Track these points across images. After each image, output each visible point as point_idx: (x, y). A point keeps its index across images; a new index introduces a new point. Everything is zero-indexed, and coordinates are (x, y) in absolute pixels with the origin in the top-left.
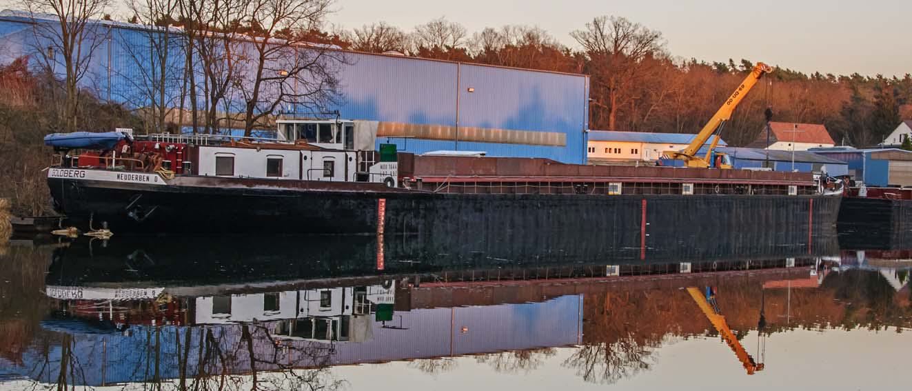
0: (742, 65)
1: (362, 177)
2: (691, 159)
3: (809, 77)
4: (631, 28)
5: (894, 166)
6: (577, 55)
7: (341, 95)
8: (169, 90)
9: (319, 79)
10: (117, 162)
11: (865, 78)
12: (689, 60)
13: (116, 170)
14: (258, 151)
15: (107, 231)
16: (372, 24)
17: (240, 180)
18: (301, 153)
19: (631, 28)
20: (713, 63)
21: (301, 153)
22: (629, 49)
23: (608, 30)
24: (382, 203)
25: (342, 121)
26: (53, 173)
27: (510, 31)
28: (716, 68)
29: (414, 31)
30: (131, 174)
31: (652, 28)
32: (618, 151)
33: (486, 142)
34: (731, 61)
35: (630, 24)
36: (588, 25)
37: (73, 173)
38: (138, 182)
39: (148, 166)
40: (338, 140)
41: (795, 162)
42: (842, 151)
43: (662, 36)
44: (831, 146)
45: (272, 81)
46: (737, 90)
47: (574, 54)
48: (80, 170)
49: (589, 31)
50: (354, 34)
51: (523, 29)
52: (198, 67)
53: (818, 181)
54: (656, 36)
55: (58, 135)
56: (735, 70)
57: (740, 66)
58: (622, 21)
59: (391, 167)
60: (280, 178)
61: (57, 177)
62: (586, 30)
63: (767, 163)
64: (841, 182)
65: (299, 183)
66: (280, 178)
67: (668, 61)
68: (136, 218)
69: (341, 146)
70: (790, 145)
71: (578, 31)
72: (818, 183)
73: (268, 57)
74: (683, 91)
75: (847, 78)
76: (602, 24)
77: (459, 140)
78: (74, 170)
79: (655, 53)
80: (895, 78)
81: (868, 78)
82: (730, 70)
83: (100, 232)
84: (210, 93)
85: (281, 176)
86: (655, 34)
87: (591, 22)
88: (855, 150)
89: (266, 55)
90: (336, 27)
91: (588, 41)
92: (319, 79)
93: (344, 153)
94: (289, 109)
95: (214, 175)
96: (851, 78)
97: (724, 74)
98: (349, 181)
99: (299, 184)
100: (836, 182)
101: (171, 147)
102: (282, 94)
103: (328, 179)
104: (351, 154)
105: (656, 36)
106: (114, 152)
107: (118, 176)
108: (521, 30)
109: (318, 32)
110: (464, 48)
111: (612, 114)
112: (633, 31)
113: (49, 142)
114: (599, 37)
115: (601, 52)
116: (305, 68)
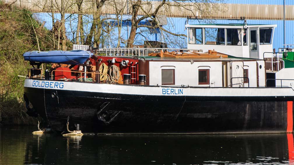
18: (257, 62)
21: (257, 62)
37: (53, 85)
48: (59, 82)
61: (38, 87)
77: (288, 19)
83: (74, 132)
113: (28, 58)
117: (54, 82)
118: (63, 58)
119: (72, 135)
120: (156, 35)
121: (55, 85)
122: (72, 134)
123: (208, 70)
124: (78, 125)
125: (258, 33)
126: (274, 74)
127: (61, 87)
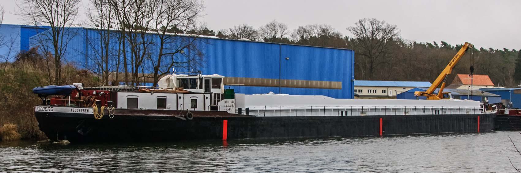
1: (215, 108)
2: (431, 96)
4: (380, 24)
6: (352, 40)
8: (110, 62)
10: (71, 102)
13: (71, 106)
14: (152, 94)
16: (239, 26)
17: (141, 111)
19: (380, 24)
23: (368, 26)
24: (225, 122)
25: (202, 76)
26: (39, 109)
28: (428, 46)
30: (79, 108)
31: (392, 24)
33: (297, 87)
34: (434, 42)
36: (356, 24)
37: (47, 109)
38: (82, 113)
39: (89, 104)
40: (201, 88)
45: (167, 55)
47: (350, 39)
48: (51, 107)
53: (483, 106)
54: (394, 28)
55: (40, 88)
59: (231, 102)
61: (39, 111)
62: (355, 26)
63: (472, 97)
64: (495, 107)
65: (177, 112)
68: (82, 133)
69: (202, 91)
71: (351, 27)
73: (165, 42)
76: (364, 22)
77: (282, 87)
78: (48, 107)
79: (394, 37)
84: (134, 63)
85: (165, 108)
86: (393, 27)
87: (358, 22)
89: (164, 41)
90: (202, 24)
93: (203, 94)
94: (174, 70)
95: (126, 108)
98: (348, 115)
99: (176, 112)
100: (493, 107)
101: (102, 93)
103: (193, 109)
104: (206, 95)
105: (394, 28)
106: (70, 97)
107: (72, 110)
109: (208, 30)
115: (364, 38)
120: (117, 78)
121: (48, 109)
127: (52, 110)
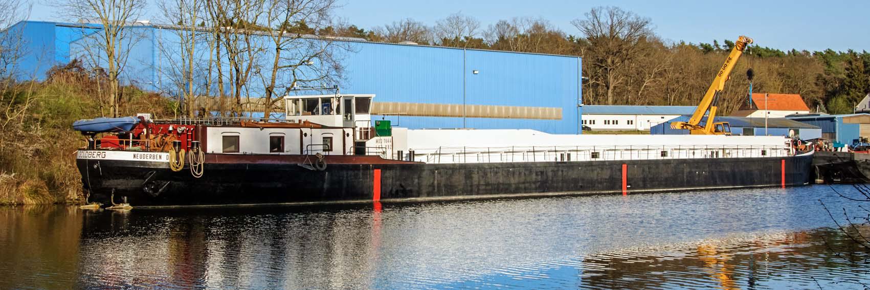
0: (725, 45)
1: (360, 148)
3: (786, 53)
5: (862, 127)
7: (346, 79)
9: (326, 66)
11: (837, 52)
12: (677, 42)
15: (127, 205)
17: (245, 156)
19: (625, 16)
20: (699, 44)
22: (623, 33)
27: (518, 22)
28: (702, 49)
29: (436, 25)
31: (643, 16)
32: (607, 123)
34: (715, 41)
35: (624, 13)
36: (586, 14)
37: (95, 154)
41: (769, 127)
42: (816, 117)
43: (653, 22)
44: (807, 112)
45: (285, 69)
46: (721, 70)
47: (577, 40)
48: (101, 152)
49: (587, 19)
50: (385, 29)
51: (529, 19)
52: (225, 60)
54: (647, 22)
56: (719, 50)
57: (724, 46)
58: (616, 10)
60: (281, 153)
65: (302, 157)
66: (281, 153)
67: (661, 45)
70: (769, 113)
72: (789, 146)
73: (284, 47)
74: (672, 68)
75: (821, 54)
77: (467, 117)
80: (864, 52)
81: (840, 52)
82: (715, 49)
83: (121, 205)
85: (283, 151)
87: (589, 11)
88: (828, 116)
91: (586, 28)
92: (326, 66)
93: (342, 129)
96: (824, 53)
97: (709, 53)
102: (295, 80)
104: (347, 131)
105: (647, 22)
107: (134, 156)
108: (528, 21)
110: (481, 38)
111: (610, 91)
112: (626, 18)
114: (596, 22)
116: (315, 56)
117: (97, 151)
118: (107, 126)
119: (118, 208)
122: (117, 207)
123: (283, 137)
124: (125, 197)
125: (354, 102)
126: (365, 142)
127: (103, 156)
